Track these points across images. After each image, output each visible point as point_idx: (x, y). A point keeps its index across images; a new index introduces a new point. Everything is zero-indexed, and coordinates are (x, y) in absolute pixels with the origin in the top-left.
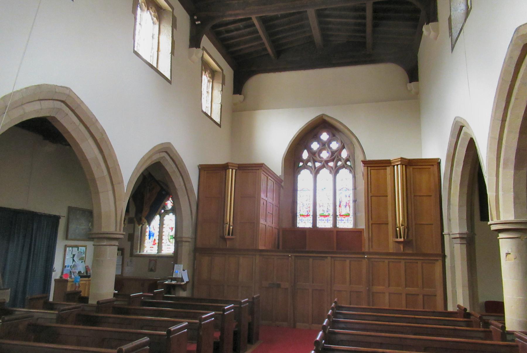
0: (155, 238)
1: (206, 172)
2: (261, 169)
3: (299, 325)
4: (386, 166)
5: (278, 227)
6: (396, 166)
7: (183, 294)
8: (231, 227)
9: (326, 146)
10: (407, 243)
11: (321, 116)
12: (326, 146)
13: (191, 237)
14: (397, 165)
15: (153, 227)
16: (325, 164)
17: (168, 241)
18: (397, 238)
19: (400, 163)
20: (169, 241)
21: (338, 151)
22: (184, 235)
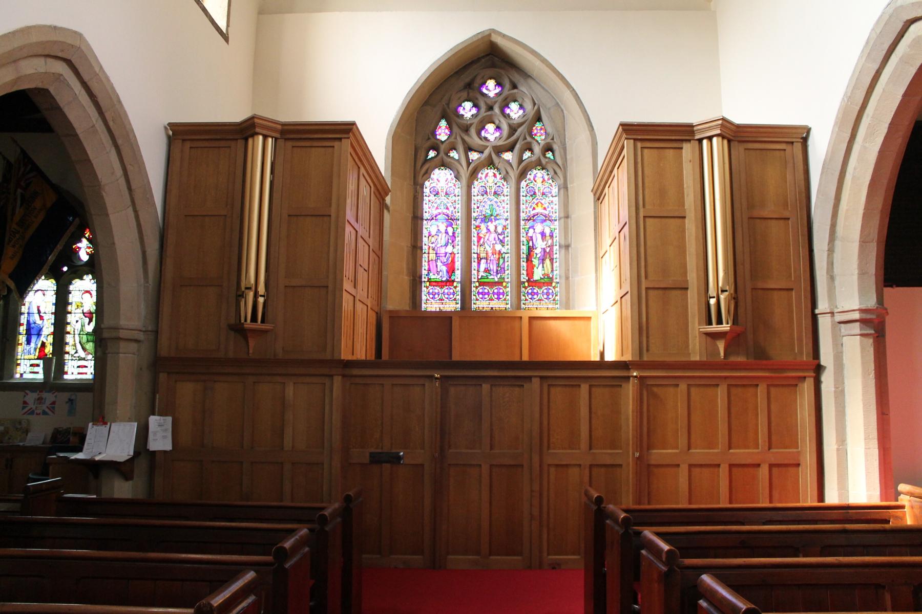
0: (45, 341)
1: (188, 145)
2: (349, 138)
3: (459, 561)
4: (682, 141)
5: (376, 309)
6: (705, 142)
7: (122, 489)
8: (261, 300)
9: (497, 110)
10: (734, 340)
11: (487, 33)
12: (497, 110)
13: (144, 329)
14: (710, 138)
15: (39, 312)
16: (494, 156)
17: (79, 347)
18: (710, 323)
19: (718, 132)
20: (84, 349)
21: (524, 125)
22: (123, 322)
